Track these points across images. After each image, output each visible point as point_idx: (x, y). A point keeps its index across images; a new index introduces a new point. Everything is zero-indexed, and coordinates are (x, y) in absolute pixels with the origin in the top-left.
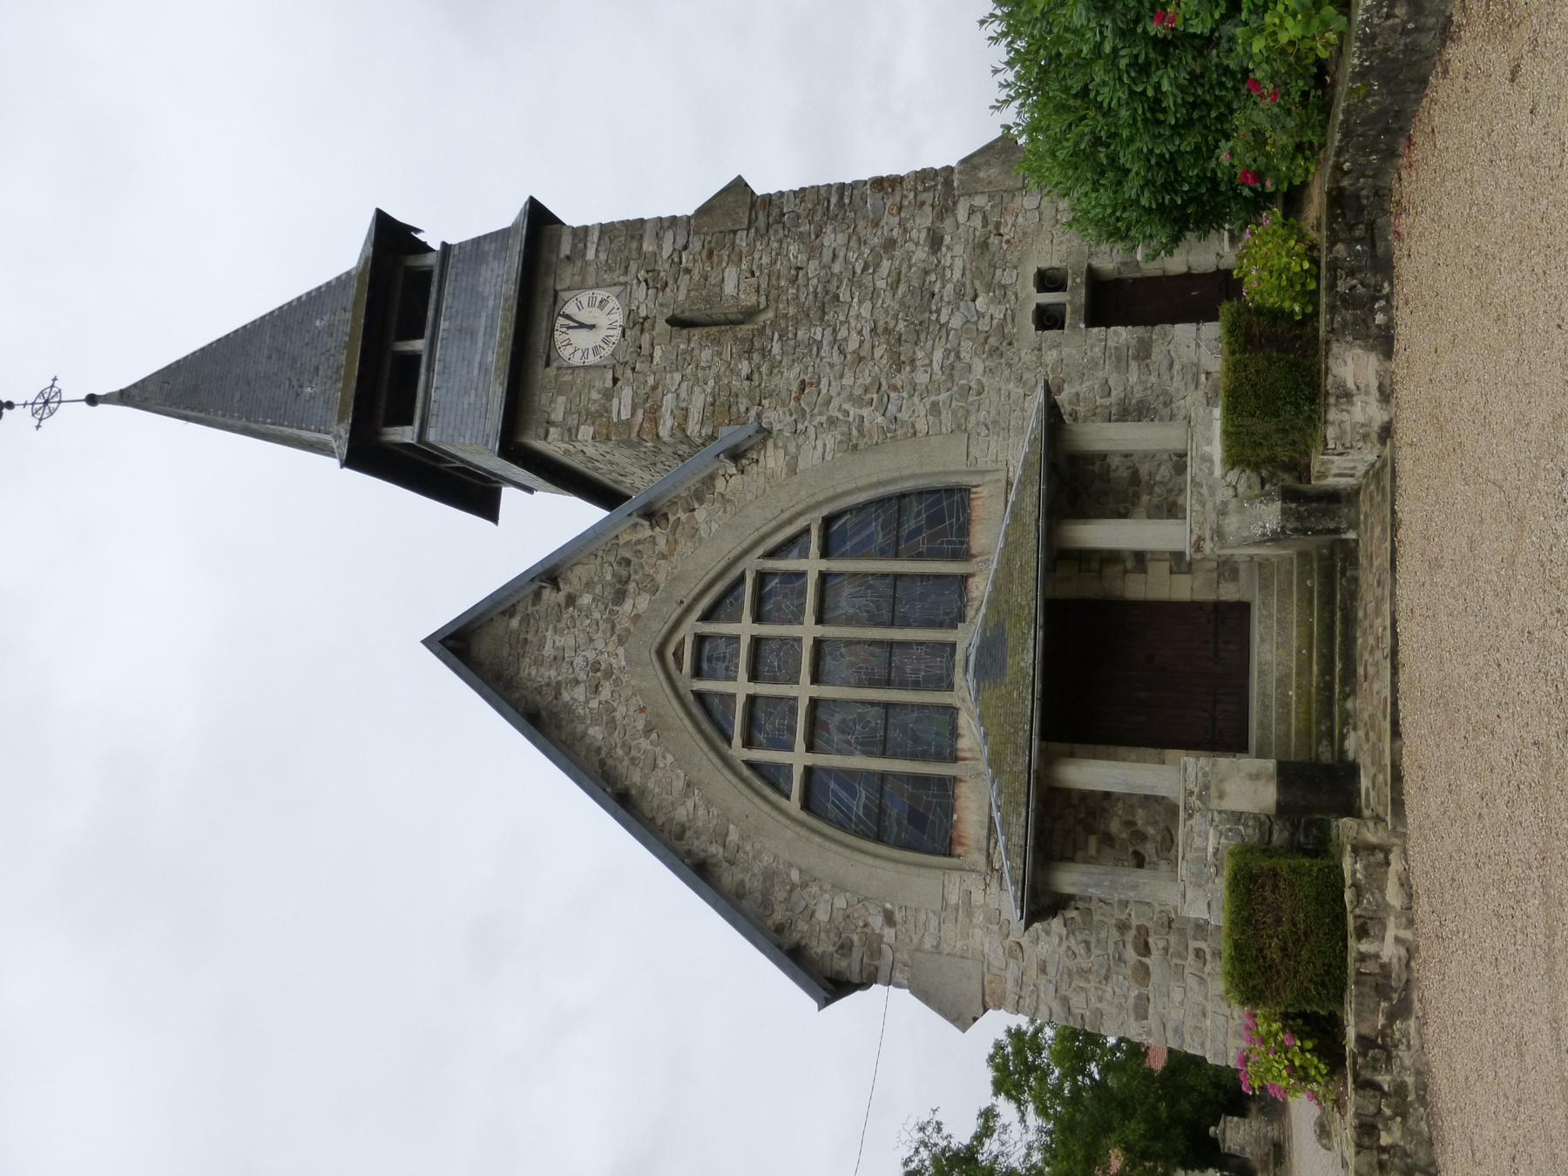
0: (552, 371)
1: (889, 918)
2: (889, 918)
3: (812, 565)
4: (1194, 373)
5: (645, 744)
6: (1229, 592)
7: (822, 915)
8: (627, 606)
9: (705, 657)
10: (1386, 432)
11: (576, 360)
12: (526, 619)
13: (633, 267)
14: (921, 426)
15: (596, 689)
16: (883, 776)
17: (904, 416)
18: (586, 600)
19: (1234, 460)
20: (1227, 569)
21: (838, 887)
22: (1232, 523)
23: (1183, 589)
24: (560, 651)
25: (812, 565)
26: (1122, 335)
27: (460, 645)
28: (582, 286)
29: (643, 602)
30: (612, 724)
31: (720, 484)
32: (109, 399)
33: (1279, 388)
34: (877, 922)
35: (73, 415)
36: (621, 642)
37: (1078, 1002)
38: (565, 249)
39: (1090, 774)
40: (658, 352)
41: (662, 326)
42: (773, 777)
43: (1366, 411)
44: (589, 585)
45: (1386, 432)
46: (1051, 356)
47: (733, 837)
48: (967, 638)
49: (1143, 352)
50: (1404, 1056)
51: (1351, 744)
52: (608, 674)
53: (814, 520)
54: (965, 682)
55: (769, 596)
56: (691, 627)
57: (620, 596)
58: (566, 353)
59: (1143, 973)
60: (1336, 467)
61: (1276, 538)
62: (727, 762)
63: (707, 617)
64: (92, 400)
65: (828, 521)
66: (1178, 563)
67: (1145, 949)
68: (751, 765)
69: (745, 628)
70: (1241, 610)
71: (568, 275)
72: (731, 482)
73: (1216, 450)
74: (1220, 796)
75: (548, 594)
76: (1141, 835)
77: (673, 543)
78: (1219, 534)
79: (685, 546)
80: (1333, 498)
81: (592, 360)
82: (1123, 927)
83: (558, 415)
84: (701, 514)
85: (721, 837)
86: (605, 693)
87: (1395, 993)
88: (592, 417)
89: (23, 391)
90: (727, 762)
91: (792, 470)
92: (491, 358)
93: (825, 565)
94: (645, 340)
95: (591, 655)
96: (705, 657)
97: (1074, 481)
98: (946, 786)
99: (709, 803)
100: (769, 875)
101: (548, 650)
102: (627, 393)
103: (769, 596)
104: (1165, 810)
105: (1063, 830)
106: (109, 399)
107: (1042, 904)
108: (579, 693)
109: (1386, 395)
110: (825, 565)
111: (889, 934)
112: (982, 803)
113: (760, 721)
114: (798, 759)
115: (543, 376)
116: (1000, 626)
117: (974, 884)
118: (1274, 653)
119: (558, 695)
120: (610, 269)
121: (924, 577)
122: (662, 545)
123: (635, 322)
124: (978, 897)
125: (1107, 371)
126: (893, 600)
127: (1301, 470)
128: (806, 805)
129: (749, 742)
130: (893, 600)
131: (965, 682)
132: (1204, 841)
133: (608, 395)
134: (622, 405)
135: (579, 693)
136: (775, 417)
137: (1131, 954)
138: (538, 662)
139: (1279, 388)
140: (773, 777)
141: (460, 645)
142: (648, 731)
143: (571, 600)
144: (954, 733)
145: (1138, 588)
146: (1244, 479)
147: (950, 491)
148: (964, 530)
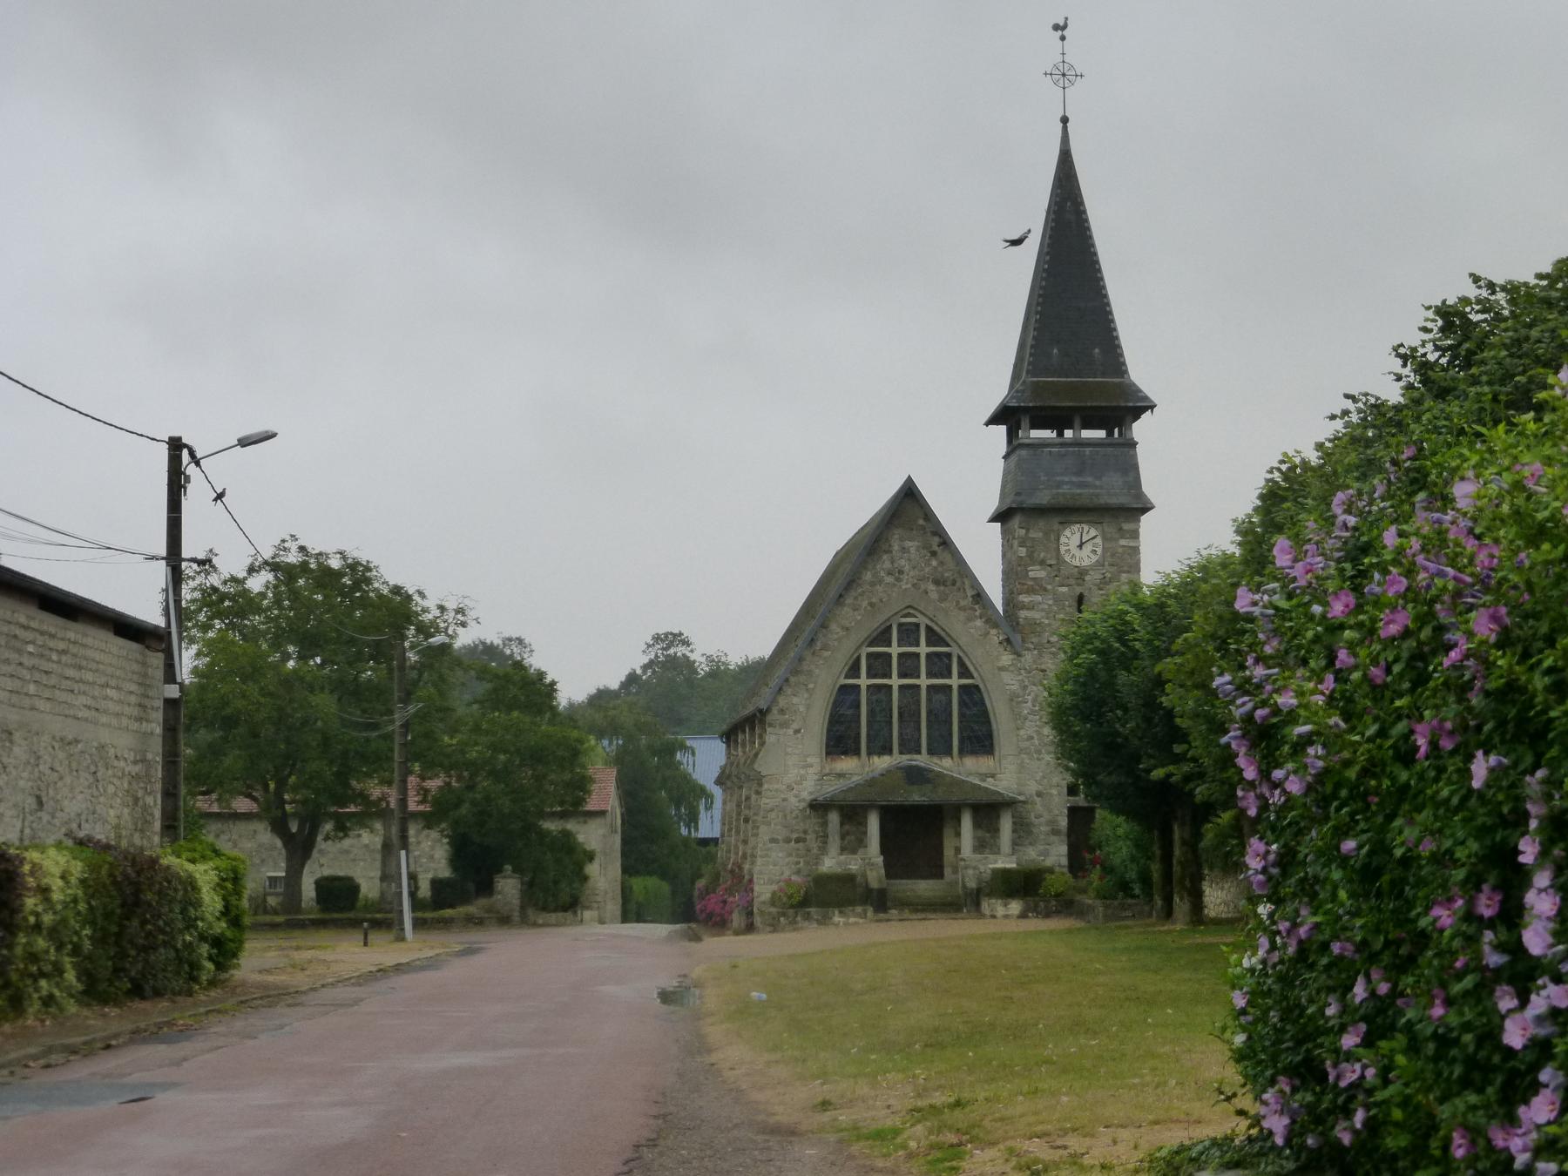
0: (1056, 526)
1: (797, 731)
2: (797, 731)
3: (955, 681)
4: (1046, 853)
5: (865, 603)
6: (947, 871)
7: (795, 700)
8: (932, 587)
9: (909, 634)
10: (994, 917)
11: (1063, 540)
12: (923, 528)
13: (1113, 569)
14: (1022, 732)
15: (889, 574)
16: (858, 722)
17: (1028, 723)
18: (934, 563)
19: (995, 872)
20: (955, 870)
21: (808, 707)
22: (970, 872)
23: (948, 852)
24: (907, 550)
25: (955, 681)
26: (1063, 823)
27: (908, 504)
28: (1104, 539)
29: (934, 595)
30: (873, 584)
31: (993, 632)
32: (1065, 129)
33: (1023, 885)
34: (795, 726)
35: (1049, 101)
36: (914, 585)
37: (773, 815)
38: (1126, 526)
39: (873, 823)
40: (1064, 589)
41: (1078, 590)
42: (854, 671)
43: (1000, 911)
44: (942, 563)
45: (994, 917)
46: (1054, 792)
47: (827, 654)
48: (922, 760)
49: (1055, 832)
50: (806, 924)
51: (894, 911)
52: (898, 580)
53: (977, 681)
54: (905, 760)
55: (940, 664)
56: (923, 621)
57: (937, 582)
58: (1067, 532)
59: (788, 841)
60: (985, 905)
61: (964, 886)
62: (859, 647)
63: (928, 628)
64: (1065, 120)
65: (977, 687)
66: (958, 850)
67: (798, 841)
68: (858, 659)
69: (923, 649)
70: (940, 876)
71: (1110, 529)
72: (995, 636)
73: (1000, 865)
74: (869, 860)
75: (936, 540)
76: (852, 843)
77: (963, 609)
78: (966, 868)
79: (962, 616)
80: (978, 905)
81: (1063, 549)
82: (805, 832)
83: (1032, 534)
84: (979, 623)
85: (825, 647)
86: (889, 579)
87: (824, 921)
88: (1030, 555)
89: (1077, 51)
90: (859, 647)
91: (1001, 669)
92: (1065, 489)
93: (955, 688)
94: (1072, 581)
95: (907, 568)
96: (909, 634)
97: (988, 810)
98: (857, 752)
99: (839, 640)
100: (810, 673)
101: (908, 544)
102: (1042, 574)
103: (940, 664)
104: (861, 842)
105: (851, 812)
106: (1065, 129)
107: (819, 807)
108: (887, 565)
109: (1006, 917)
110: (955, 688)
111: (791, 732)
112: (856, 769)
113: (880, 665)
114: (863, 681)
115: (1054, 522)
116: (928, 781)
117: (816, 769)
118: (924, 887)
119: (886, 552)
120: (1113, 555)
121: (951, 735)
122: (963, 603)
123: (1082, 573)
124: (811, 770)
125: (1046, 816)
126: (939, 718)
127: (990, 895)
128: (843, 687)
129: (869, 655)
130: (939, 718)
131: (905, 760)
132: (854, 865)
133: (1042, 563)
134: (1037, 572)
135: (887, 565)
136: (1028, 657)
137: (795, 836)
138: (901, 539)
139: (1023, 885)
140: (854, 671)
141: (908, 504)
142: (872, 605)
143: (934, 554)
144: (880, 754)
145: (948, 834)
146: (987, 876)
147: (992, 745)
148: (974, 753)
